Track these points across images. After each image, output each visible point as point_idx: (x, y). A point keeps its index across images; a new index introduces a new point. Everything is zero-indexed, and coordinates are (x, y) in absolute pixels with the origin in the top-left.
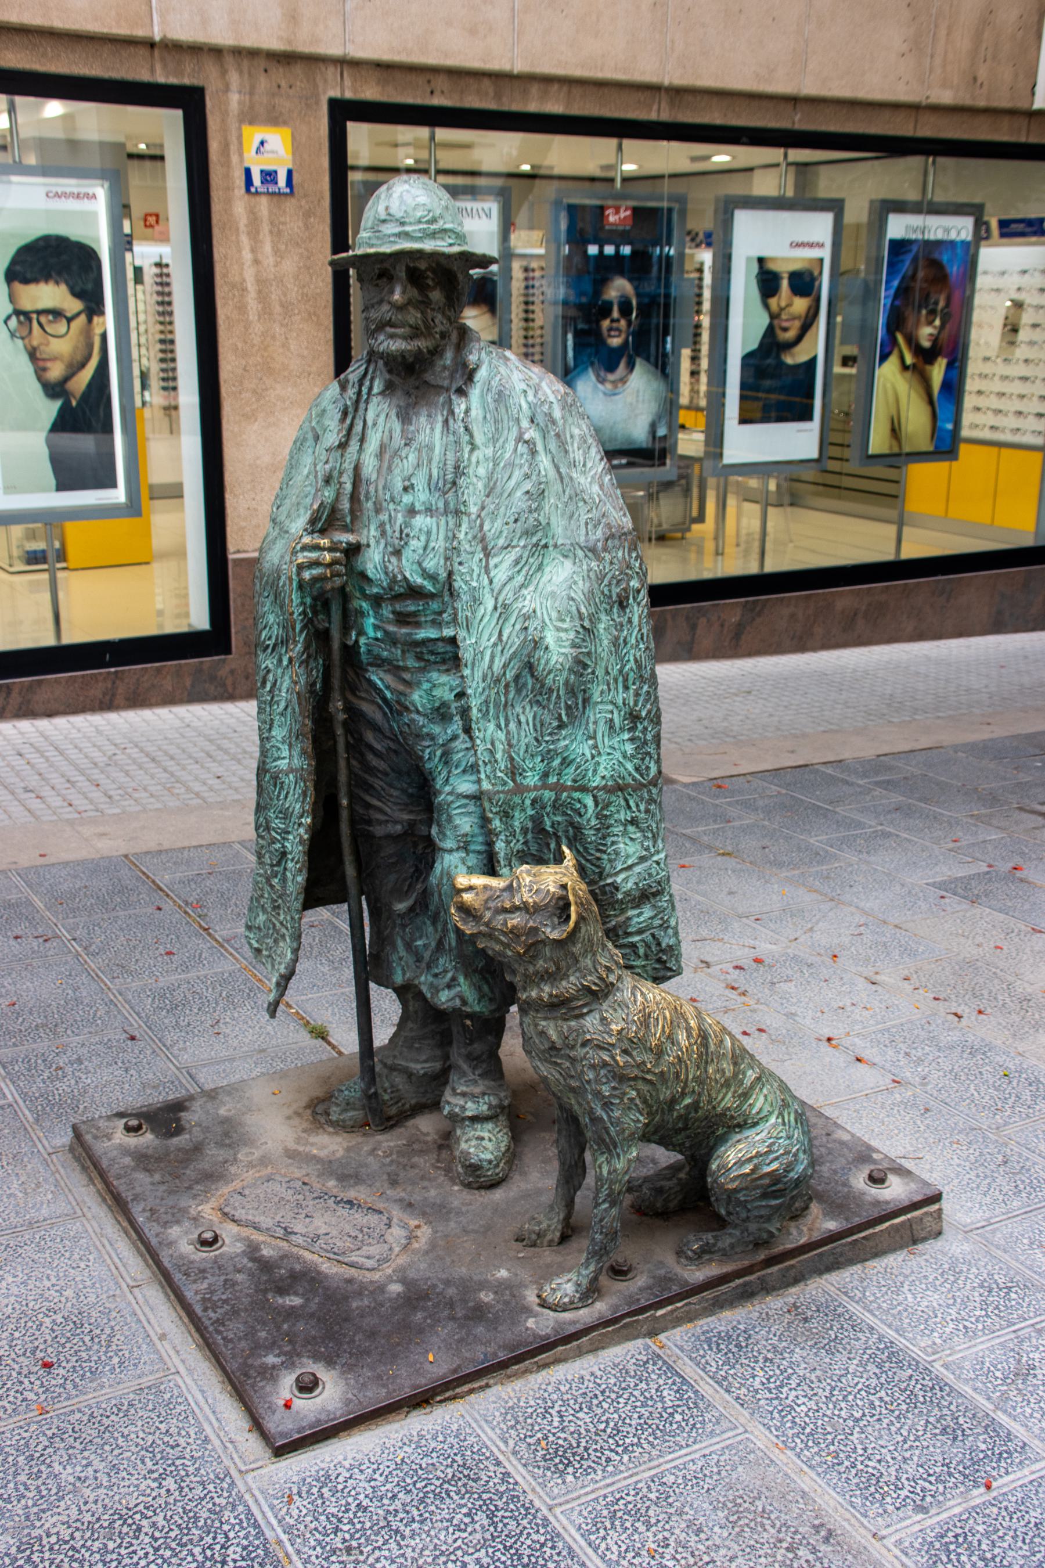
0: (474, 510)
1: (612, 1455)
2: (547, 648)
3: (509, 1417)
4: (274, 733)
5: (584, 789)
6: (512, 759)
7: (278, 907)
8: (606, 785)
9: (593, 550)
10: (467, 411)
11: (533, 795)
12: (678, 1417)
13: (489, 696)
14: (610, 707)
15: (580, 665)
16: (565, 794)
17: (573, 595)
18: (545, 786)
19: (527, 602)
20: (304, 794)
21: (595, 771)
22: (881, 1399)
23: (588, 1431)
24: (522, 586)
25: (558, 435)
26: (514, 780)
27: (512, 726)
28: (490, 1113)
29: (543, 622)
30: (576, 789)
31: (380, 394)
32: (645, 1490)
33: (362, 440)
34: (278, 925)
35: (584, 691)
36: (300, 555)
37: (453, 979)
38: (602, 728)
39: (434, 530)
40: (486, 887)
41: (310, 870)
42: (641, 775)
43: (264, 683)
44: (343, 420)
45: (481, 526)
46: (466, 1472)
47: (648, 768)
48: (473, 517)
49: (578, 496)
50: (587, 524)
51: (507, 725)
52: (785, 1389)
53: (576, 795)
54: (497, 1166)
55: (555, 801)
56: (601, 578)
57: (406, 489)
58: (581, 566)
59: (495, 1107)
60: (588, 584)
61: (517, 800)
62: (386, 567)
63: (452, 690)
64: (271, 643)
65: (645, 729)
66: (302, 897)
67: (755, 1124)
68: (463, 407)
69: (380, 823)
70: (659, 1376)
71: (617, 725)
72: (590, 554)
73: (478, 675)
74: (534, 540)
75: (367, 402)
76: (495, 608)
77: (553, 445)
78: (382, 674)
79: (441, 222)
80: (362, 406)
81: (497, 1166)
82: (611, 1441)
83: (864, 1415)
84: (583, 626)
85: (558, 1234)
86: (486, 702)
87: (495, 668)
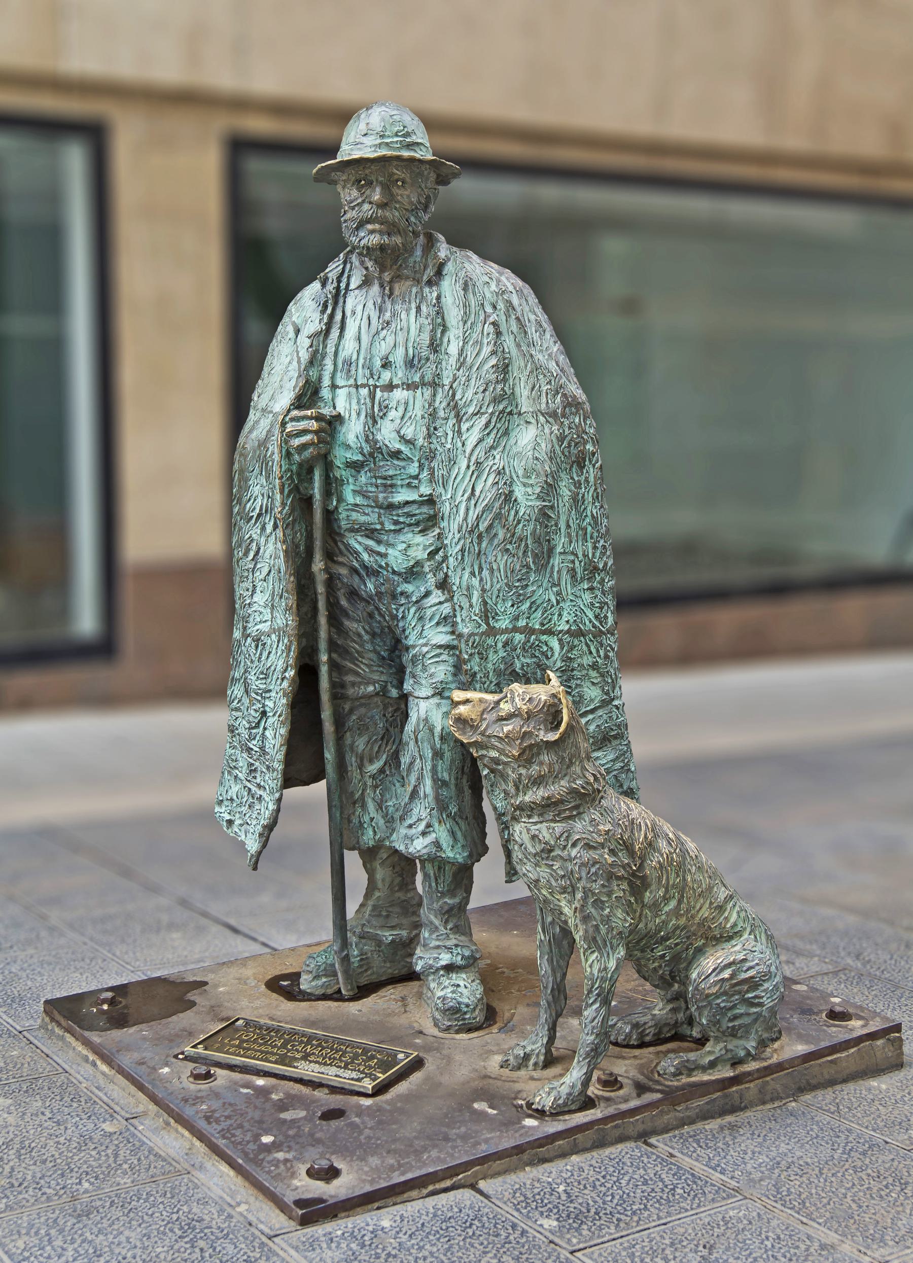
0: (446, 382)
1: (623, 1217)
2: (515, 500)
3: (518, 1195)
4: (255, 599)
5: (550, 632)
6: (485, 603)
7: (255, 770)
8: (569, 629)
9: (554, 415)
10: (439, 298)
11: (504, 637)
12: (679, 1191)
13: (464, 545)
14: (572, 558)
15: (544, 515)
16: (533, 637)
17: (537, 455)
18: (515, 629)
19: (496, 461)
20: (288, 649)
21: (560, 615)
22: (869, 1175)
23: (595, 1202)
24: (492, 448)
25: (518, 319)
26: (488, 624)
27: (485, 573)
28: (463, 963)
29: (511, 477)
30: (544, 633)
31: (359, 287)
32: (658, 1238)
33: (342, 328)
34: (253, 789)
35: (549, 541)
36: (288, 425)
37: (429, 826)
38: (565, 577)
39: (411, 402)
40: (481, 701)
41: (292, 723)
42: (601, 623)
43: (247, 551)
44: (323, 312)
45: (454, 395)
46: (485, 1231)
47: (606, 617)
48: (447, 388)
49: (537, 368)
50: (547, 394)
51: (480, 572)
52: (776, 1171)
53: (544, 638)
54: (474, 1009)
55: (525, 643)
56: (561, 439)
57: (384, 366)
58: (543, 431)
59: (468, 957)
60: (549, 446)
61: (490, 641)
62: (367, 436)
63: (425, 550)
64: (255, 514)
65: (603, 580)
66: (284, 749)
67: (730, 938)
68: (435, 294)
69: (353, 684)
70: (656, 1165)
71: (579, 576)
72: (550, 420)
73: (454, 527)
74: (501, 407)
75: (345, 296)
76: (468, 467)
77: (514, 327)
78: (359, 539)
79: (414, 137)
80: (341, 300)
81: (474, 1009)
82: (619, 1208)
83: (854, 1184)
84: (546, 482)
85: (542, 1058)
86: (462, 551)
87: (469, 521)
